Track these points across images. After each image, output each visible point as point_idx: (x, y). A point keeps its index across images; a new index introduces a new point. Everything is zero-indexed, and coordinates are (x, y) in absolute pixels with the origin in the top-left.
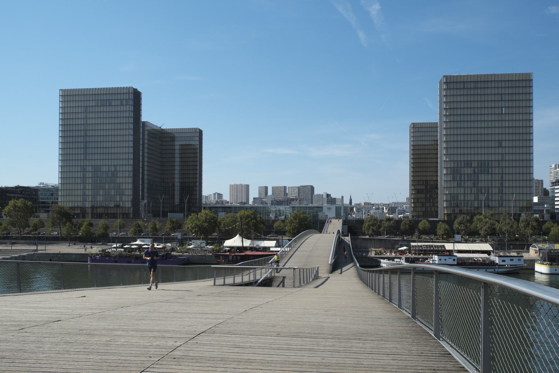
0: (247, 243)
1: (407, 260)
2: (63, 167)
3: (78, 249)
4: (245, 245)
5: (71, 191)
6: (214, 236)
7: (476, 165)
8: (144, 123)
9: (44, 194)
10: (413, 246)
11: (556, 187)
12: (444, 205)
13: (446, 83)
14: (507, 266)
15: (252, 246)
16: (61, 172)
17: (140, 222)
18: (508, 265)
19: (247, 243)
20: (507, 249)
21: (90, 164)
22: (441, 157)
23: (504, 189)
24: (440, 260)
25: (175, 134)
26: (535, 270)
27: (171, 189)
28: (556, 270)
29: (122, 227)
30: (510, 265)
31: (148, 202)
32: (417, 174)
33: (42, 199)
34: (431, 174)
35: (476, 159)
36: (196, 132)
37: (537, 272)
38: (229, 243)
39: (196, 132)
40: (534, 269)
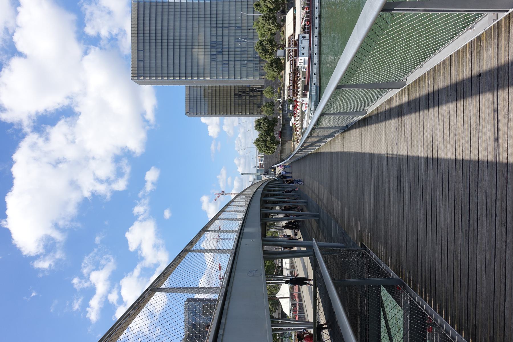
1: (304, 95)
7: (214, 50)
10: (289, 96)
13: (138, 77)
22: (208, 82)
24: (303, 54)
34: (225, 101)
35: (209, 50)
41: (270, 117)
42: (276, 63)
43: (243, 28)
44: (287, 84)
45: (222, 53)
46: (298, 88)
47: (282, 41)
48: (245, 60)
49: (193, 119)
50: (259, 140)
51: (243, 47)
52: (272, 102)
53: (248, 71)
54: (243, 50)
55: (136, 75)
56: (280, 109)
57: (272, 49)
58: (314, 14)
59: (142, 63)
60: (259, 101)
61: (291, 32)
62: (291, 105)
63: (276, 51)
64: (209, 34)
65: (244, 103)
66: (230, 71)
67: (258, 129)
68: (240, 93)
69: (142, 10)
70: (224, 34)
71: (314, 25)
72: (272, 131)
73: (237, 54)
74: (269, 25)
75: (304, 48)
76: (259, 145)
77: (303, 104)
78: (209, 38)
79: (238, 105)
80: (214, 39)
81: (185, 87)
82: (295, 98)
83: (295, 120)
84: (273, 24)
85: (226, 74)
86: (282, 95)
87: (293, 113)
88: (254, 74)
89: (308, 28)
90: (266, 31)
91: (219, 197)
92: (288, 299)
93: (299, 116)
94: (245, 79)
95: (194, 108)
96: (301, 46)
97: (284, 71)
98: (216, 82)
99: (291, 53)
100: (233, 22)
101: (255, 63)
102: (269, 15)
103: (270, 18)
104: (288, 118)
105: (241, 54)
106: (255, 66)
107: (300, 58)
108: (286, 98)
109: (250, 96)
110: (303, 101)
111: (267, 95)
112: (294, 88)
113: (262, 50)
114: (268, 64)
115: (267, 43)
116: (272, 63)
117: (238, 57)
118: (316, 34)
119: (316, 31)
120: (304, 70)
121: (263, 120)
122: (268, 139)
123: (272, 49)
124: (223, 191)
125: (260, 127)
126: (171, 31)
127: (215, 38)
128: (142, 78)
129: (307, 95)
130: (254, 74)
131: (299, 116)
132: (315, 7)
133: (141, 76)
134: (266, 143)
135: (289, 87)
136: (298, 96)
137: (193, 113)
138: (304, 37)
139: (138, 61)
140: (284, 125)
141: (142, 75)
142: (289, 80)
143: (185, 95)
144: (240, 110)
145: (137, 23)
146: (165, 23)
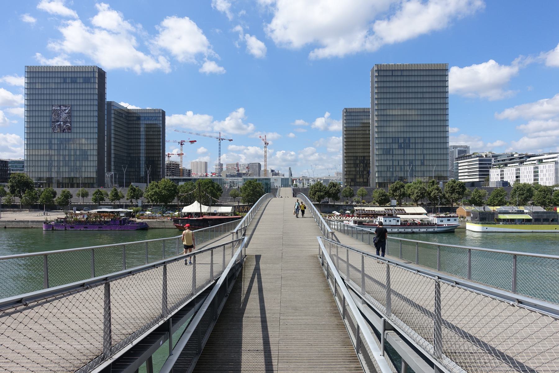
0: (205, 209)
1: (355, 222)
2: (29, 140)
3: (37, 216)
4: (202, 211)
5: (37, 162)
6: (173, 203)
7: (402, 141)
8: (110, 104)
9: (14, 166)
10: (357, 210)
11: (459, 162)
12: (376, 175)
13: (378, 71)
14: (444, 226)
15: (209, 212)
16: (27, 144)
17: (102, 190)
18: (445, 225)
19: (205, 209)
20: (440, 212)
21: (56, 137)
22: (373, 134)
23: (425, 161)
24: (386, 221)
25: (140, 114)
26: (467, 229)
27: (136, 163)
28: (487, 228)
29: (85, 195)
30: (448, 225)
31: (115, 174)
32: (439, 90)
33: (13, 171)
35: (402, 136)
36: (159, 113)
37: (467, 230)
38: (187, 209)
39: (159, 113)
40: (466, 228)
41: (340, 195)
42: (385, 199)
43: (422, 167)
44: (367, 209)
45: (400, 148)
46: (363, 217)
47: (405, 203)
48: (393, 169)
49: (341, 114)
50: (321, 186)
51: (405, 167)
52: (353, 195)
53: (383, 172)
54: (403, 167)
55: (379, 69)
56: (347, 203)
57: (396, 196)
58: (415, 228)
59: (391, 74)
60: (358, 180)
61: (407, 212)
62: (349, 212)
63: (396, 199)
64: (416, 136)
65: (356, 165)
66: (383, 156)
67: (330, 185)
68: (366, 162)
69: (439, 73)
70: (417, 150)
71: (406, 228)
72: (329, 197)
73: (398, 162)
74: (417, 193)
75: (390, 221)
76: (317, 185)
77: (349, 221)
78: (414, 136)
79: (354, 160)
80: (412, 141)
81: (369, 107)
82: (355, 215)
83: (337, 215)
84: (417, 196)
85: (381, 152)
86: (359, 204)
87: (343, 214)
88: (380, 178)
89: (404, 224)
90: (411, 190)
91: (263, 140)
92: (200, 211)
93: (340, 218)
94: (376, 169)
95: (351, 117)
96: (392, 219)
97: (378, 205)
98: (373, 138)
99: (391, 212)
100: (428, 158)
101: (391, 178)
102: (425, 193)
103: (422, 194)
104: (339, 210)
105: (398, 165)
106: (388, 178)
107: (382, 218)
108: (355, 208)
109: (363, 172)
110: (351, 221)
111: (361, 190)
112: (362, 215)
113: (396, 188)
114: (385, 193)
115: (402, 191)
116: (385, 195)
117: (396, 163)
118: (400, 230)
119: (402, 230)
120: (374, 222)
121: (337, 189)
122: (322, 193)
123: (396, 196)
124: (268, 144)
125: (332, 187)
126: (419, 101)
127: (414, 141)
128: (376, 74)
129: (356, 224)
130: (380, 178)
131: (340, 218)
132: (420, 229)
133: (378, 74)
134: (319, 191)
135: (364, 210)
136: (356, 218)
137: (346, 116)
138: (398, 221)
139: (392, 70)
140: (333, 206)
141: (380, 75)
142: (369, 211)
143: (364, 107)
144: (349, 162)
145: (427, 69)
146: (427, 95)
